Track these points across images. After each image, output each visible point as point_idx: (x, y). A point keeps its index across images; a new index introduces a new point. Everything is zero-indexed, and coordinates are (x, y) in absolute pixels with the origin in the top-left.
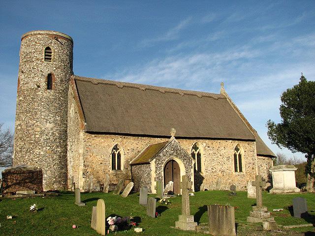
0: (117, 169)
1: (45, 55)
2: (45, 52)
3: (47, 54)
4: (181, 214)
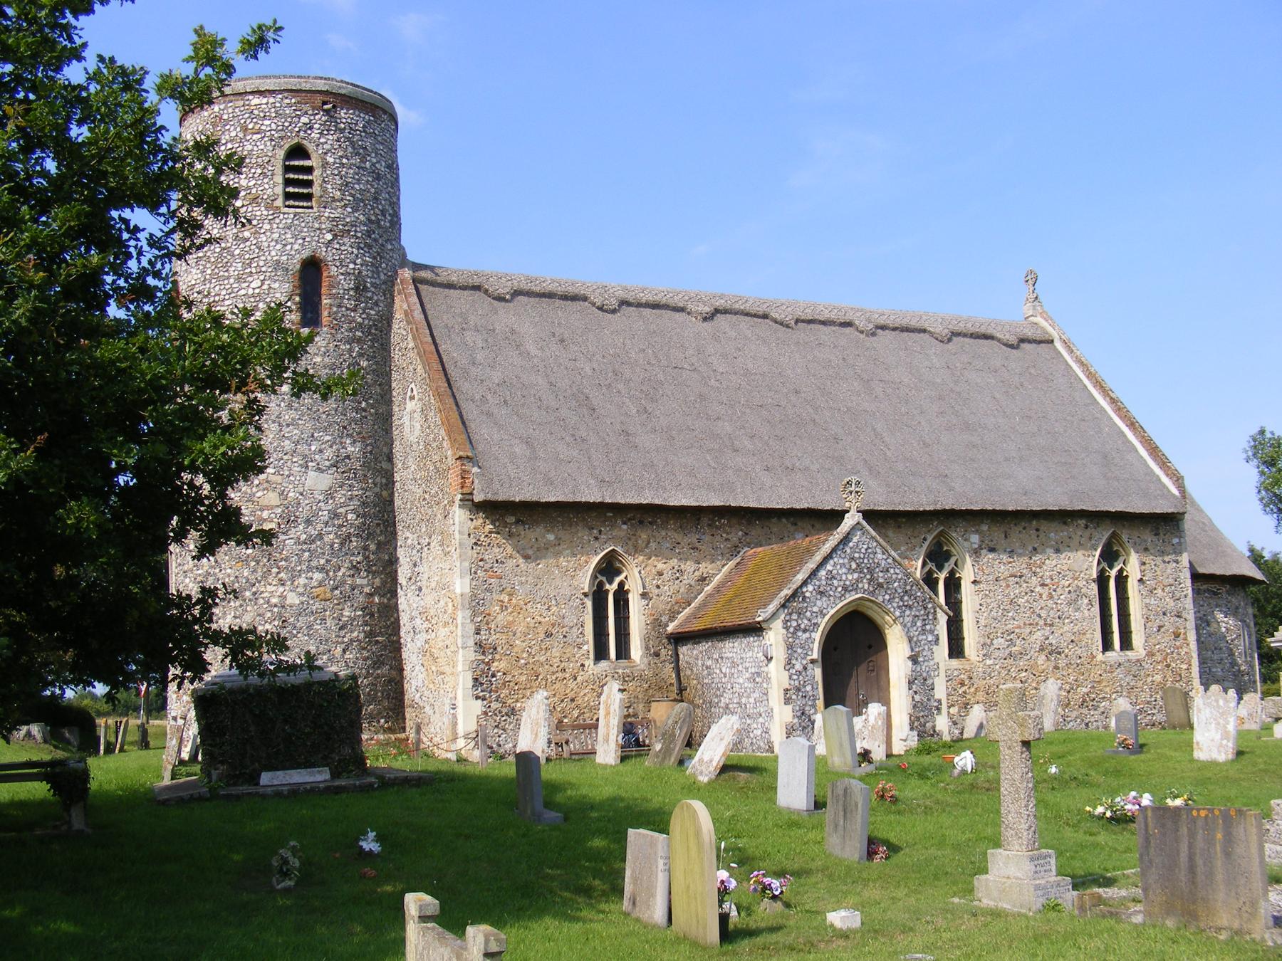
1: (288, 182)
2: (288, 169)
3: (291, 189)
4: (997, 844)
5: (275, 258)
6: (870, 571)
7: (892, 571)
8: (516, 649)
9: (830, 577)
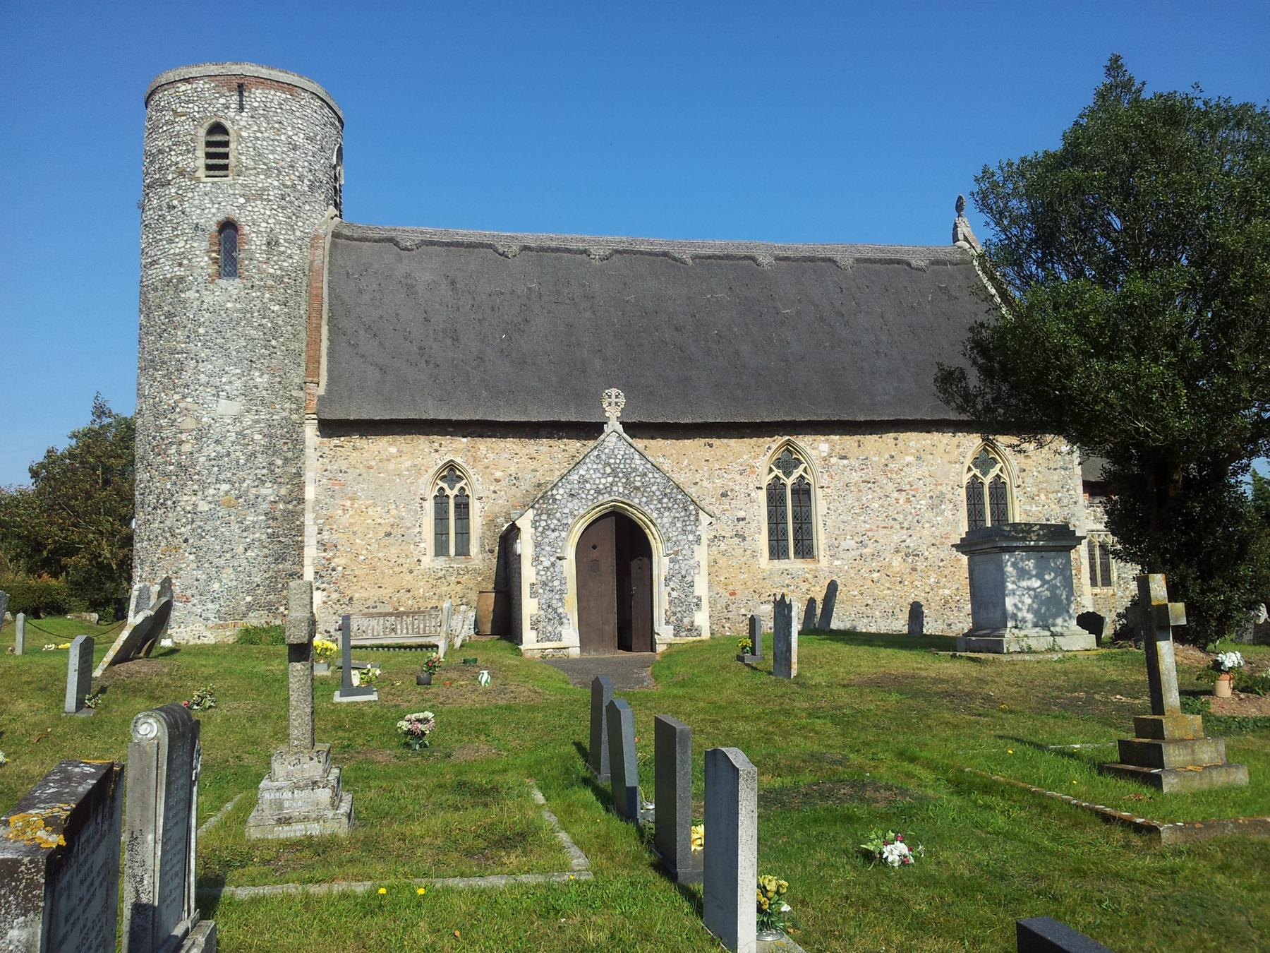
0: (452, 551)
1: (209, 156)
2: (209, 144)
5: (195, 222)
6: (627, 476)
7: (650, 475)
8: (356, 547)
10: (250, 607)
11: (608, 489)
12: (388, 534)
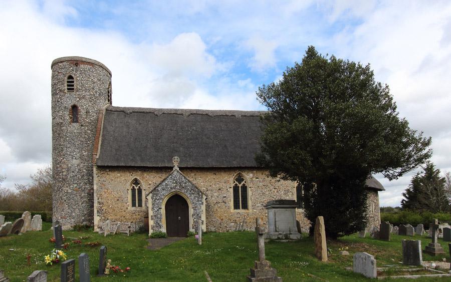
1: (68, 85)
6: (180, 183)
9: (167, 185)
10: (84, 221)
11: (175, 188)
12: (118, 200)
